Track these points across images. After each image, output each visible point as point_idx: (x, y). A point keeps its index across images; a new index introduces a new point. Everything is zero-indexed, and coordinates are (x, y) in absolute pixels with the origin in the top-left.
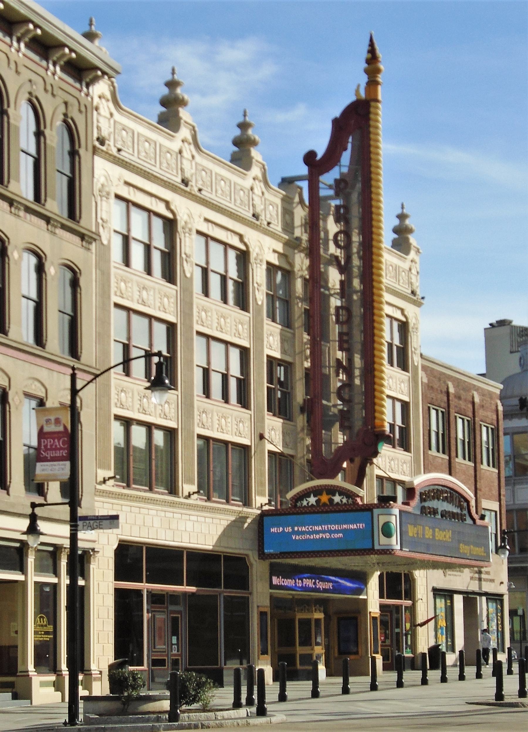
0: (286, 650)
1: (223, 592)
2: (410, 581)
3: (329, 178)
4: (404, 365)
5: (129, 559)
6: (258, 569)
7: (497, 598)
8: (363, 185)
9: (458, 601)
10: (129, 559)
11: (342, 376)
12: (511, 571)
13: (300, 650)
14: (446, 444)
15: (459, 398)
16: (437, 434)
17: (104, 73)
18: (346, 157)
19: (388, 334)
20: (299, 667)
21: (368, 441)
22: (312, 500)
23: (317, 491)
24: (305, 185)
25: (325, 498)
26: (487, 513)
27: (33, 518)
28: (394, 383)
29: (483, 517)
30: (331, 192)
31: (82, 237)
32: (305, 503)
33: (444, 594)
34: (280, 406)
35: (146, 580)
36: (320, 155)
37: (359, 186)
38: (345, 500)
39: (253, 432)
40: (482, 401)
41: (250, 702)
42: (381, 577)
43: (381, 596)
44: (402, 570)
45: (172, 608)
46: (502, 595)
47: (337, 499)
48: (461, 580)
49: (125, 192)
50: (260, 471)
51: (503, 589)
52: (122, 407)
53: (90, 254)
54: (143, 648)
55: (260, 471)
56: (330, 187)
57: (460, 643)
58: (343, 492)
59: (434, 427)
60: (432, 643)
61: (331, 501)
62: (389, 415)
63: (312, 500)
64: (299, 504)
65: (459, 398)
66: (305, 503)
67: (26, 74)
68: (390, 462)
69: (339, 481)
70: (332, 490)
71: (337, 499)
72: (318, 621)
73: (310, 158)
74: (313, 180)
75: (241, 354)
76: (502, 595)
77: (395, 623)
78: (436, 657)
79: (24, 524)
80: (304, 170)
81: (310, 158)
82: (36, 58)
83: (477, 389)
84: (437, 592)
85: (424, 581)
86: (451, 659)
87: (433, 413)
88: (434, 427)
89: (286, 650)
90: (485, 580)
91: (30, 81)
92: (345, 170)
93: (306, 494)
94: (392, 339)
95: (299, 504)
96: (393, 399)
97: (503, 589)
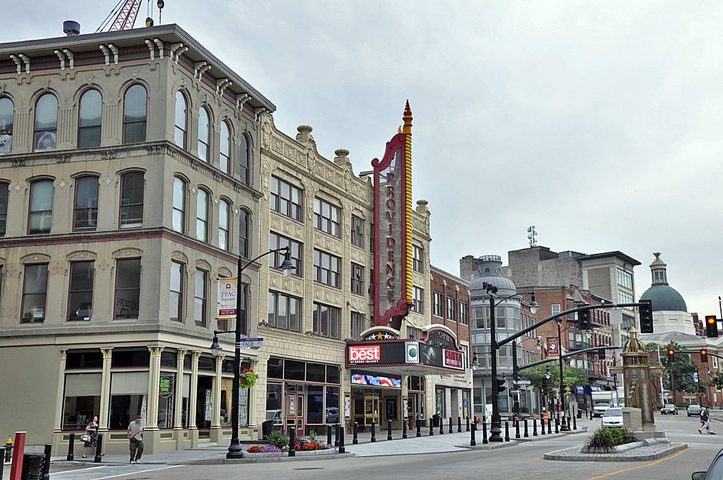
0: (359, 416)
1: (326, 385)
2: (423, 380)
3: (384, 173)
4: (421, 271)
5: (275, 366)
6: (344, 373)
7: (468, 390)
8: (402, 178)
9: (448, 392)
10: (275, 366)
11: (390, 275)
12: (474, 377)
13: (367, 416)
14: (442, 311)
15: (449, 289)
16: (438, 305)
17: (267, 109)
18: (393, 163)
19: (413, 253)
20: (366, 425)
21: (406, 307)
22: (374, 337)
23: (376, 332)
24: (372, 176)
25: (380, 336)
26: (463, 347)
27: (215, 340)
28: (415, 279)
29: (461, 348)
30: (385, 181)
31: (254, 195)
32: (370, 339)
33: (440, 388)
34: (357, 289)
35: (210, 370)
36: (380, 161)
37: (399, 179)
38: (390, 337)
39: (134, 232)
40: (460, 290)
41: (336, 445)
42: (409, 378)
43: (409, 388)
44: (420, 375)
45: (298, 392)
46: (470, 389)
47: (386, 336)
48: (449, 381)
49: (277, 173)
50: (346, 320)
51: (471, 386)
52: (317, 298)
53: (257, 204)
54: (55, 412)
55: (346, 320)
56: (384, 177)
57: (449, 414)
58: (389, 333)
59: (436, 303)
60: (435, 413)
61: (383, 337)
62: (413, 295)
63: (374, 337)
64: (367, 339)
65: (449, 289)
66: (370, 339)
67: (203, 91)
68: (412, 319)
69: (388, 328)
70: (384, 332)
71: (386, 336)
72: (376, 401)
73: (375, 162)
74: (376, 174)
75: (338, 261)
76: (470, 389)
77: (415, 402)
78: (436, 421)
79: (210, 344)
80: (372, 169)
81: (375, 162)
82: (229, 98)
83: (458, 284)
84: (438, 387)
85: (432, 381)
86: (446, 422)
87: (436, 295)
88: (436, 303)
89: (359, 416)
90: (209, 340)
91: (206, 95)
92: (393, 169)
93: (370, 334)
94: (416, 256)
95: (367, 339)
96: (417, 287)
97: (471, 386)
